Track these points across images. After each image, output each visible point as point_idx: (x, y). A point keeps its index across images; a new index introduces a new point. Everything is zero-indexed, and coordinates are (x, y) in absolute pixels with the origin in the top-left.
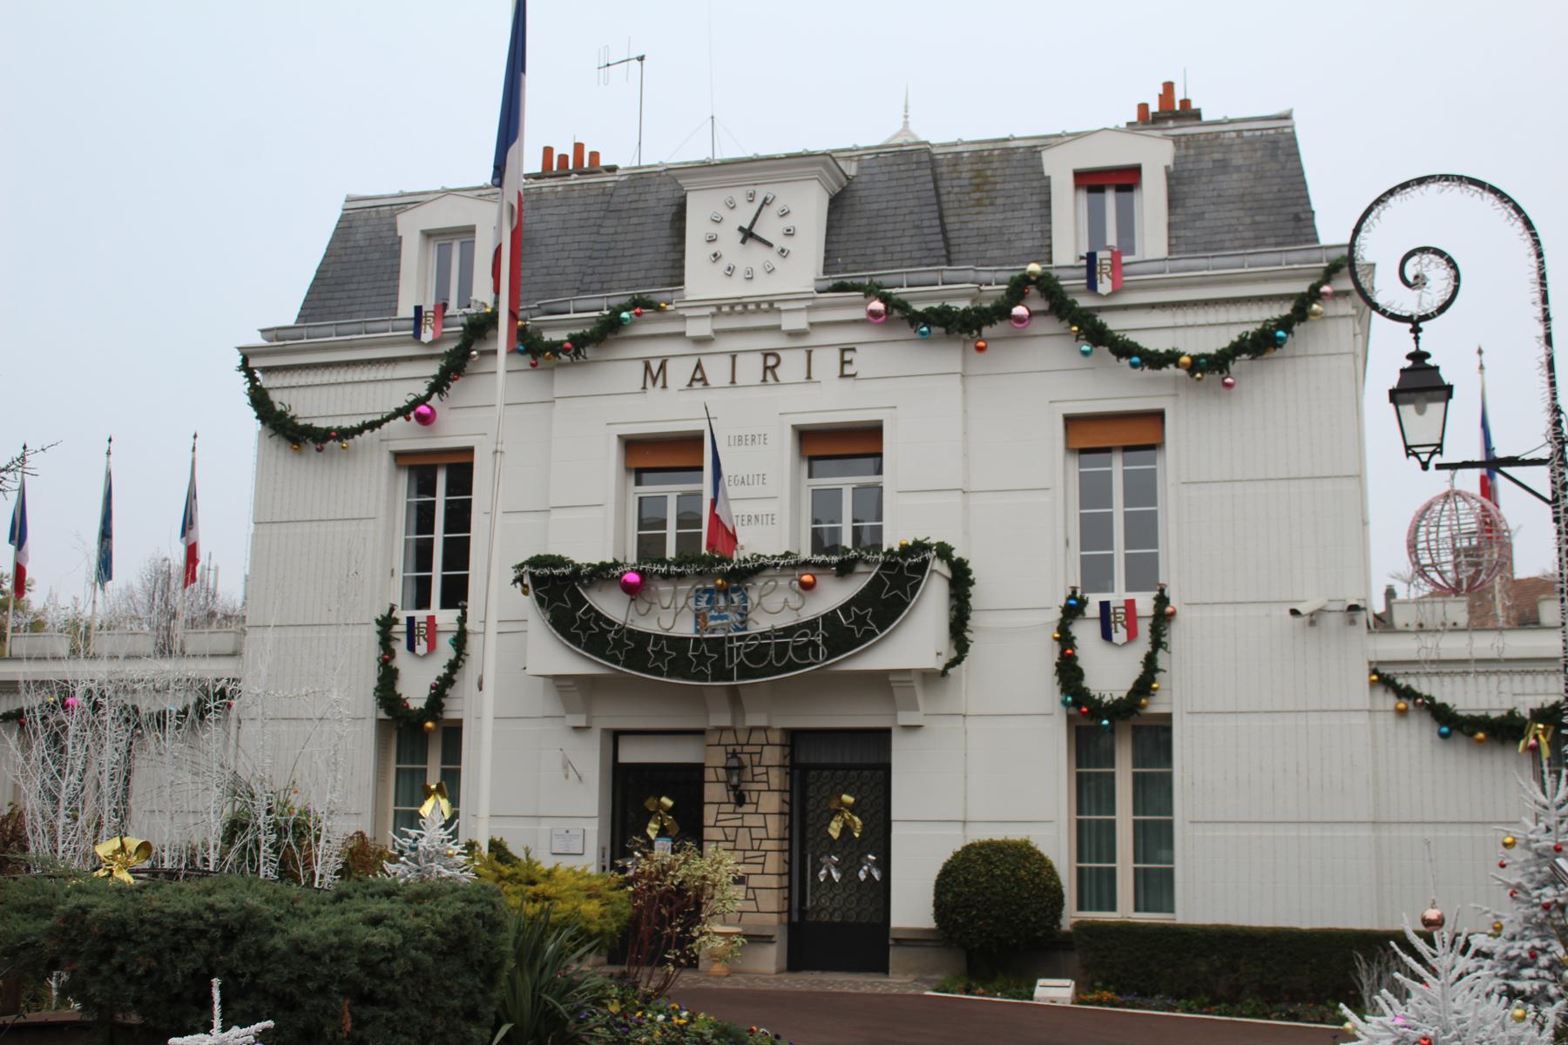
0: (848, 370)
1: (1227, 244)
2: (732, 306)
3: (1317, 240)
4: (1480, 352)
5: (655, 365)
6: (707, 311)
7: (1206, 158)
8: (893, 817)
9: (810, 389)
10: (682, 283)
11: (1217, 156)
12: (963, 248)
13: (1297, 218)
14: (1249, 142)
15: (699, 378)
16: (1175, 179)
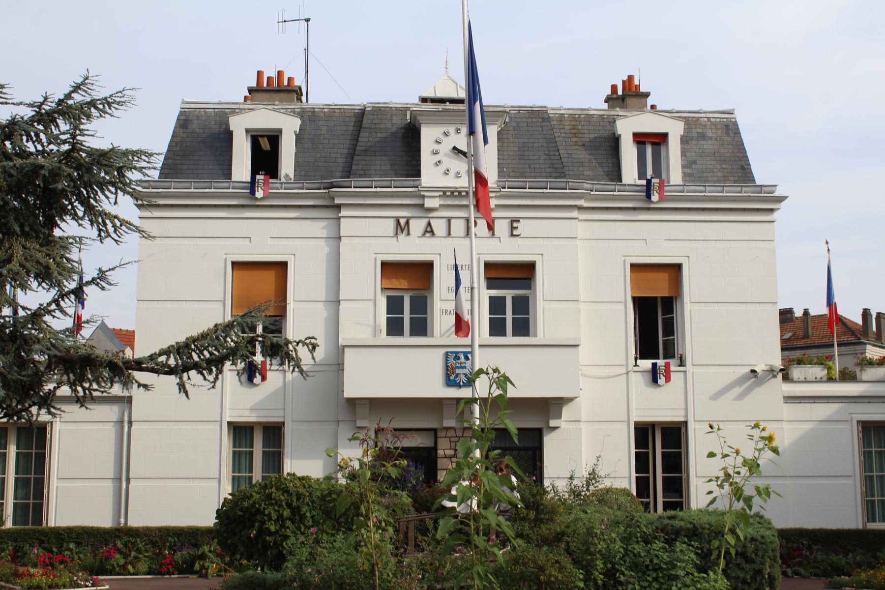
0: (515, 233)
1: (710, 179)
2: (452, 193)
3: (754, 181)
4: (827, 243)
5: (403, 222)
6: (437, 194)
7: (694, 131)
8: (105, 521)
11: (699, 130)
12: (571, 168)
13: (742, 168)
14: (713, 124)
15: (429, 230)
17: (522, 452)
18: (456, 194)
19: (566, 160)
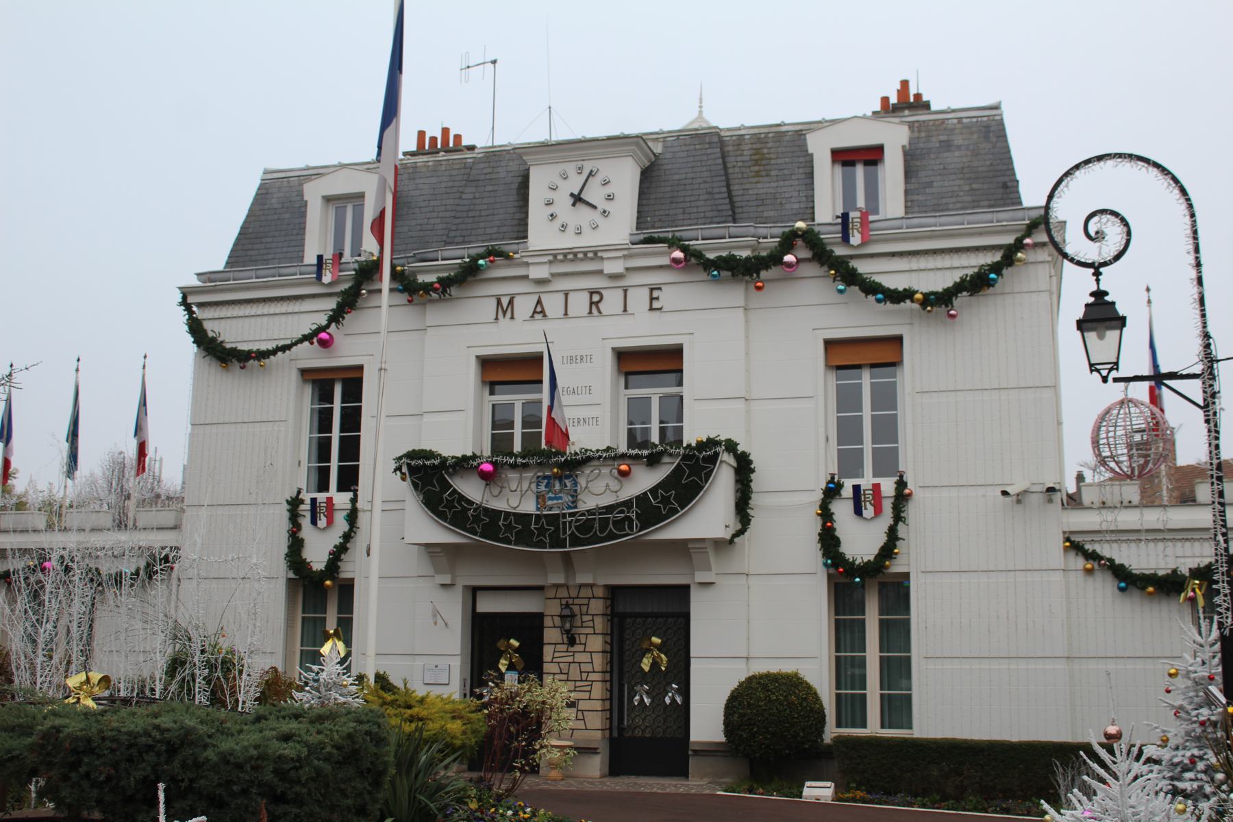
0: (656, 305)
1: (951, 206)
2: (565, 255)
3: (1020, 203)
4: (1148, 290)
5: (505, 301)
6: (545, 259)
7: (934, 139)
9: (627, 320)
10: (526, 237)
11: (942, 138)
12: (745, 209)
13: (1005, 186)
15: (539, 311)
16: (911, 157)
17: (670, 620)
18: (570, 256)
19: (739, 198)
